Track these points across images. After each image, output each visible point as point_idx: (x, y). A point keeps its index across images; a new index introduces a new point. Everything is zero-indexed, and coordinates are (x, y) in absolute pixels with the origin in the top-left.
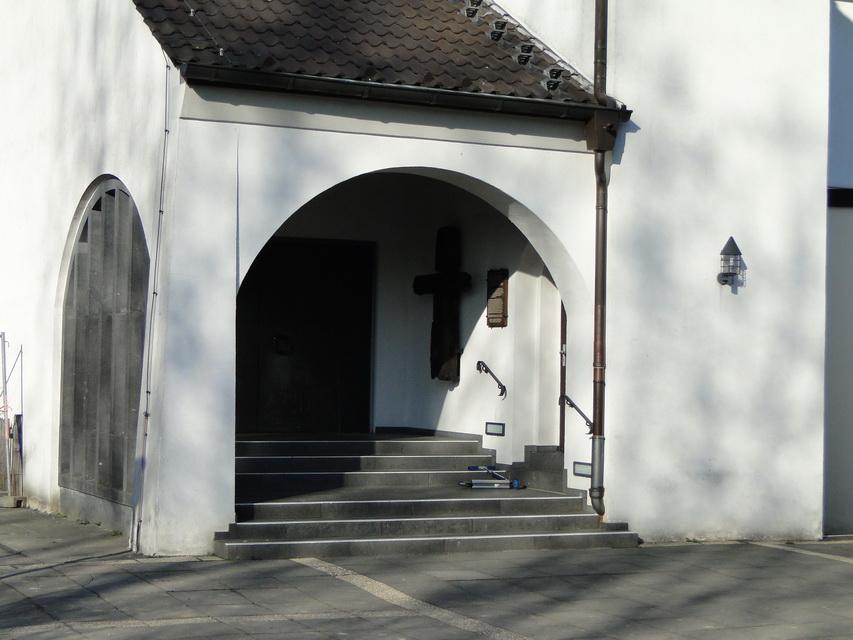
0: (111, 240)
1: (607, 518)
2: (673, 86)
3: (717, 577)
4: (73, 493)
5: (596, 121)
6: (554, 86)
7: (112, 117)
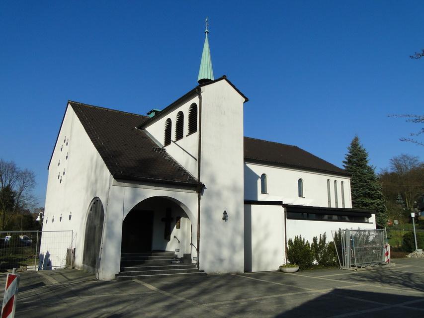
0: (97, 211)
1: (200, 270)
2: (213, 180)
3: (221, 282)
4: (85, 265)
5: (198, 187)
6: (190, 180)
7: (98, 185)
